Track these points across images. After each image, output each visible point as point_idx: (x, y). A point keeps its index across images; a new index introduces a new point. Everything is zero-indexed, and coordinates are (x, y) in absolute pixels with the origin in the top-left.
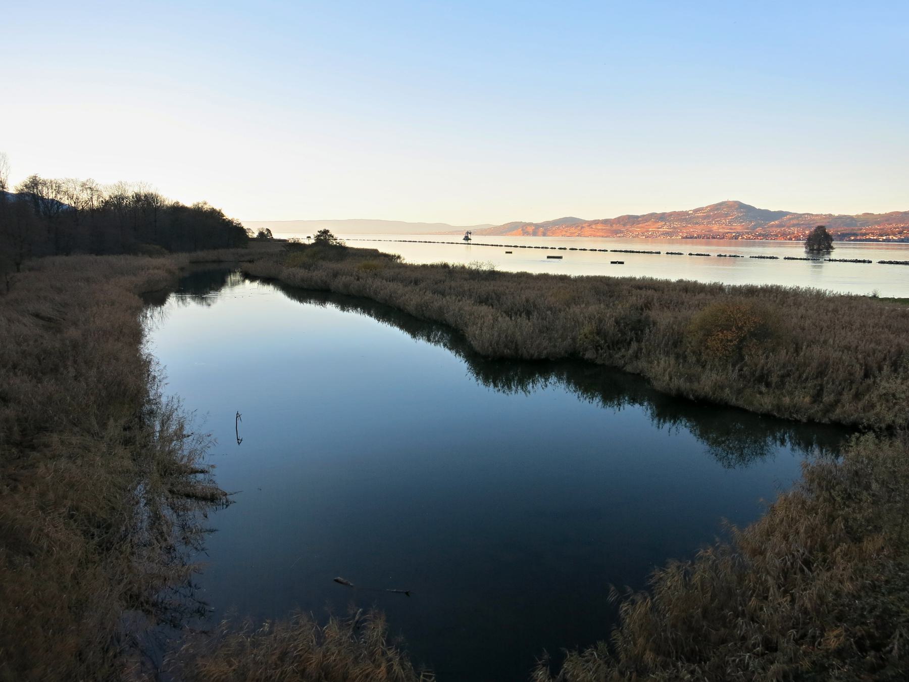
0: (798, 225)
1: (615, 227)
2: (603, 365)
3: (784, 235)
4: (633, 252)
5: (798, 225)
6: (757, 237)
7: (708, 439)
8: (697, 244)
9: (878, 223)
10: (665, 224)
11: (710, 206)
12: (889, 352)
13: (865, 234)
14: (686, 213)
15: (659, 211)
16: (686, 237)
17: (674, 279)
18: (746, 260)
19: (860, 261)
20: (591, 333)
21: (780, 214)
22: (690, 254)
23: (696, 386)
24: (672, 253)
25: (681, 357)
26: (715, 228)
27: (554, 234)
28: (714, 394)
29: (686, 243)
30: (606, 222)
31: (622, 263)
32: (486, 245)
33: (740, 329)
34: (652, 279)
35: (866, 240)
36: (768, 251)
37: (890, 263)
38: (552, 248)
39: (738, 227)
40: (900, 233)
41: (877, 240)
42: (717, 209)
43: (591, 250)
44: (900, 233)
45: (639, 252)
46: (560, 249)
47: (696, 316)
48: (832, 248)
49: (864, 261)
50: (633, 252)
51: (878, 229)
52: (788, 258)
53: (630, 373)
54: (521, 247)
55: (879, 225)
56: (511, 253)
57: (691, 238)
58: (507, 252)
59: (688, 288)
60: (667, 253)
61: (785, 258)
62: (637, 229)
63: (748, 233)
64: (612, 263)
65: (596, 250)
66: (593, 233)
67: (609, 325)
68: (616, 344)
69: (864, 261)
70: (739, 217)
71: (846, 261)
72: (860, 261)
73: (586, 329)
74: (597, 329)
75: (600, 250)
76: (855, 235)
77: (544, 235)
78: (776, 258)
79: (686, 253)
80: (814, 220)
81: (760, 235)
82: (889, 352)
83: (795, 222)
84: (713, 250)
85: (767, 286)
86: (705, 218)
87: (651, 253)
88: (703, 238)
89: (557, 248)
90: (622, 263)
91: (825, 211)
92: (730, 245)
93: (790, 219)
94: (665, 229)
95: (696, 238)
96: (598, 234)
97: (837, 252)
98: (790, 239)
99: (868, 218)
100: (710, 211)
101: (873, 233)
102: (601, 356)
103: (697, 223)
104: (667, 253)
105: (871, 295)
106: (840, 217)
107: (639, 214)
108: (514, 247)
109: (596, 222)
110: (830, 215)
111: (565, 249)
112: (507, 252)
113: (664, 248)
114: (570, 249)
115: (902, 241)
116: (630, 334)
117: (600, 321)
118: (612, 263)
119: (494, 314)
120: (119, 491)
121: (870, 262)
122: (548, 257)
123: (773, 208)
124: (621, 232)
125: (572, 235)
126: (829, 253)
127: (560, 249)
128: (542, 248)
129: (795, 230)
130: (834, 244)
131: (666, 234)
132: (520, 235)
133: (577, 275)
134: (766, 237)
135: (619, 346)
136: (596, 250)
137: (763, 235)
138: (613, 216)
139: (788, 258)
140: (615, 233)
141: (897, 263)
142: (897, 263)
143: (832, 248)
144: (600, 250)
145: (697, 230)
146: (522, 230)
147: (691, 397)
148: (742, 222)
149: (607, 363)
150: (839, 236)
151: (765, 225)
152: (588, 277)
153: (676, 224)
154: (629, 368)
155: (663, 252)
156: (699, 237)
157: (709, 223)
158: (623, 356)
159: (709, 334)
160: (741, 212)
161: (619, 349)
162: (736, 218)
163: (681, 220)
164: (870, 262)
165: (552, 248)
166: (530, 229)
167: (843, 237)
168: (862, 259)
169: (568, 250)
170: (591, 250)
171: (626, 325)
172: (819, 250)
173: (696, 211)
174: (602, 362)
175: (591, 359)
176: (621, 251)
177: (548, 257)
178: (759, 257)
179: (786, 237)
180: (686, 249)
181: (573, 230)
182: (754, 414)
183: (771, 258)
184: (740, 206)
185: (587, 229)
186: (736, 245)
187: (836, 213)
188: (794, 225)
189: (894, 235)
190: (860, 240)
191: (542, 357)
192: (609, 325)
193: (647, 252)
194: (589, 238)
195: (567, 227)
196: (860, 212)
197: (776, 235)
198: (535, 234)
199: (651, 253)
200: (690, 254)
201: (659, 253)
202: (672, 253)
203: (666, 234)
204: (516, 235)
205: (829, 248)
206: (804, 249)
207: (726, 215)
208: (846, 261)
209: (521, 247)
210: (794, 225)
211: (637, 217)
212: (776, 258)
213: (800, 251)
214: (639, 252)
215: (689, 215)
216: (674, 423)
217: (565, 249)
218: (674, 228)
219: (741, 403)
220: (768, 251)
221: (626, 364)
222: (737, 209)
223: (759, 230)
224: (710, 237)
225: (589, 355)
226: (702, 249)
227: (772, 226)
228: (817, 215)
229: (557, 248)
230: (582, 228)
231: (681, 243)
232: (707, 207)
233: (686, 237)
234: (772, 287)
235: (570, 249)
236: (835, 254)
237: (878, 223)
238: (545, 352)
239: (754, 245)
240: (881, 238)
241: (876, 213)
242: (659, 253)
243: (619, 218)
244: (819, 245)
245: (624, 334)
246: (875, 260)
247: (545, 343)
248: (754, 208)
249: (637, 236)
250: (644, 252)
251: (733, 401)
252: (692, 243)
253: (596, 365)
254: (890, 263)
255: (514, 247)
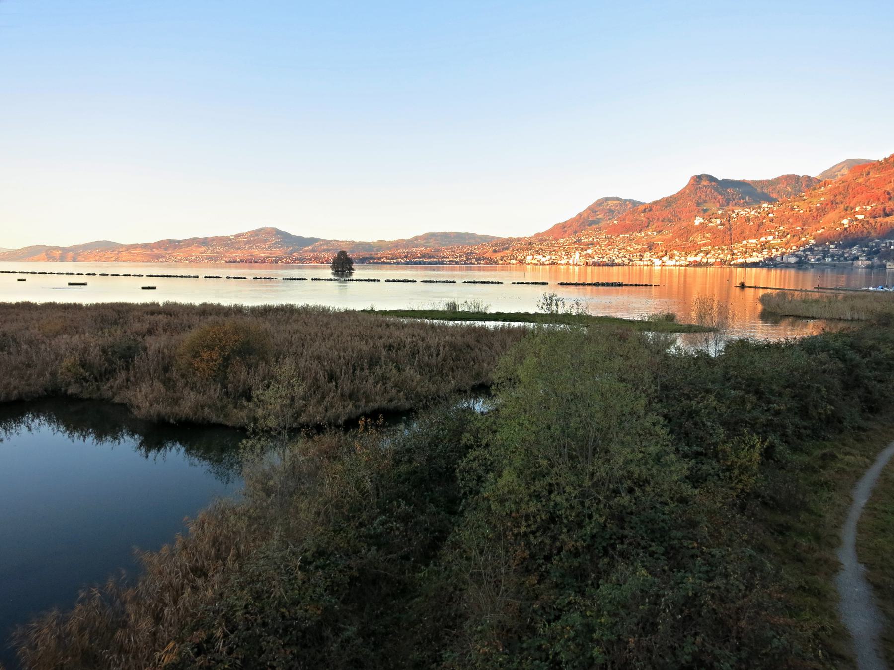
0: (328, 250)
1: (156, 251)
2: (90, 399)
3: (317, 259)
4: (170, 276)
5: (328, 250)
6: (294, 261)
7: (210, 459)
8: (241, 268)
9: (390, 249)
10: (208, 249)
11: (250, 232)
12: (352, 357)
13: (380, 258)
14: (228, 238)
15: (201, 235)
16: (230, 262)
17: (197, 302)
18: (279, 282)
19: (371, 281)
20: (74, 365)
21: (313, 241)
22: (228, 278)
23: (176, 409)
24: (210, 277)
25: (168, 383)
26: (257, 253)
27: (86, 259)
28: (195, 414)
29: (230, 267)
30: (145, 246)
31: (154, 288)
32: (168, 276)
33: (223, 349)
34: (176, 304)
35: (382, 263)
36: (296, 273)
37: (394, 281)
38: (78, 274)
39: (277, 252)
40: (406, 256)
41: (389, 263)
42: (257, 235)
43: (125, 275)
44: (406, 256)
45: (177, 277)
46: (89, 275)
47: (189, 337)
48: (353, 270)
49: (374, 281)
50: (170, 276)
51: (389, 254)
52: (315, 280)
53: (118, 404)
54: (40, 273)
55: (390, 250)
56: (24, 280)
57: (234, 262)
58: (19, 280)
59: (206, 310)
60: (206, 277)
61: (313, 280)
62: (180, 253)
63: (286, 257)
64: (143, 288)
65: (129, 276)
66: (131, 257)
67: (94, 354)
68: (108, 374)
69: (374, 281)
70: (277, 242)
71: (361, 281)
72: (371, 281)
73: (67, 362)
74: (81, 361)
75: (135, 276)
76: (373, 258)
77: (74, 259)
78: (305, 280)
79: (224, 277)
80: (340, 246)
81: (297, 259)
82: (352, 357)
83: (325, 247)
84: (248, 273)
85: (282, 305)
86: (248, 242)
87: (189, 277)
88: (246, 262)
89: (85, 274)
90: (154, 288)
91: (349, 238)
92: (271, 269)
93: (321, 245)
94: (209, 253)
95: (239, 262)
96: (138, 259)
97: (358, 272)
98: (323, 263)
99: (382, 245)
100: (251, 236)
101: (386, 257)
102: (87, 389)
103: (239, 248)
104: (206, 277)
105: (369, 309)
106: (361, 244)
107: (181, 239)
108: (32, 273)
109: (134, 246)
110: (353, 242)
111: (94, 275)
112: (19, 280)
113: (202, 273)
114: (101, 275)
115: (408, 263)
116: (120, 363)
117: (86, 350)
118: (143, 288)
119: (505, 412)
120: (666, 517)
121: (379, 281)
122: (70, 284)
123: (306, 235)
124: (163, 257)
125: (107, 260)
126: (351, 274)
127: (89, 275)
128: (67, 274)
129: (326, 255)
130: (354, 266)
131: (210, 258)
132: (44, 260)
133: (142, 302)
134: (302, 261)
135: (107, 377)
136: (129, 276)
137: (299, 259)
138: (153, 240)
139: (315, 280)
140: (157, 257)
141: (399, 281)
142: (399, 281)
143: (353, 270)
144: (135, 276)
145: (239, 254)
146: (47, 254)
147: (172, 421)
148: (280, 247)
149: (95, 396)
150: (360, 259)
151: (301, 249)
152: (103, 304)
153: (220, 249)
154: (117, 399)
155: (201, 276)
156: (242, 261)
157: (250, 248)
158: (112, 387)
159: (196, 355)
160: (278, 238)
161: (108, 380)
162: (275, 243)
163: (224, 245)
164: (379, 281)
165: (78, 274)
166: (57, 254)
167: (363, 260)
168: (373, 279)
169: (98, 276)
170: (125, 275)
171: (114, 353)
172: (343, 272)
173: (237, 236)
174: (89, 396)
175: (76, 394)
176: (157, 276)
177: (70, 284)
178: (290, 279)
179: (318, 260)
180: (223, 273)
181: (109, 254)
182: (234, 428)
183: (300, 279)
184: (278, 232)
185: (125, 253)
186: (277, 269)
187: (357, 240)
188: (324, 250)
189: (402, 258)
190: (377, 263)
191: (13, 399)
192: (94, 354)
193: (185, 277)
194: (128, 263)
195: (102, 251)
196: (376, 240)
197: (311, 259)
198: (62, 258)
199: (189, 277)
200: (228, 278)
201: (197, 277)
202: (210, 277)
203: (210, 258)
204: (38, 260)
205: (351, 270)
206: (330, 271)
207: (266, 241)
208: (361, 281)
209: (40, 273)
210: (324, 250)
211: (179, 242)
212: (305, 280)
213: (328, 273)
214: (177, 277)
215: (230, 240)
216: (159, 450)
217: (94, 275)
218: (217, 252)
219: (221, 420)
220: (296, 273)
221: (114, 394)
222: (274, 235)
223: (296, 254)
224: (253, 261)
225: (72, 390)
226: (234, 272)
227: (306, 251)
228: (343, 242)
229: (85, 274)
230: (119, 252)
231: (225, 267)
232: (247, 233)
233: (230, 262)
234: (286, 305)
235: (101, 275)
236: (356, 275)
237: (390, 249)
238: (16, 392)
239: (292, 268)
240: (393, 261)
241: (387, 240)
242: (197, 277)
243: (159, 242)
244: (343, 267)
245: (111, 362)
246: (383, 280)
247: (14, 382)
248: (289, 235)
249: (180, 260)
250: (182, 277)
251: (214, 418)
252: (236, 267)
253: (82, 400)
254: (394, 281)
255: (32, 273)
